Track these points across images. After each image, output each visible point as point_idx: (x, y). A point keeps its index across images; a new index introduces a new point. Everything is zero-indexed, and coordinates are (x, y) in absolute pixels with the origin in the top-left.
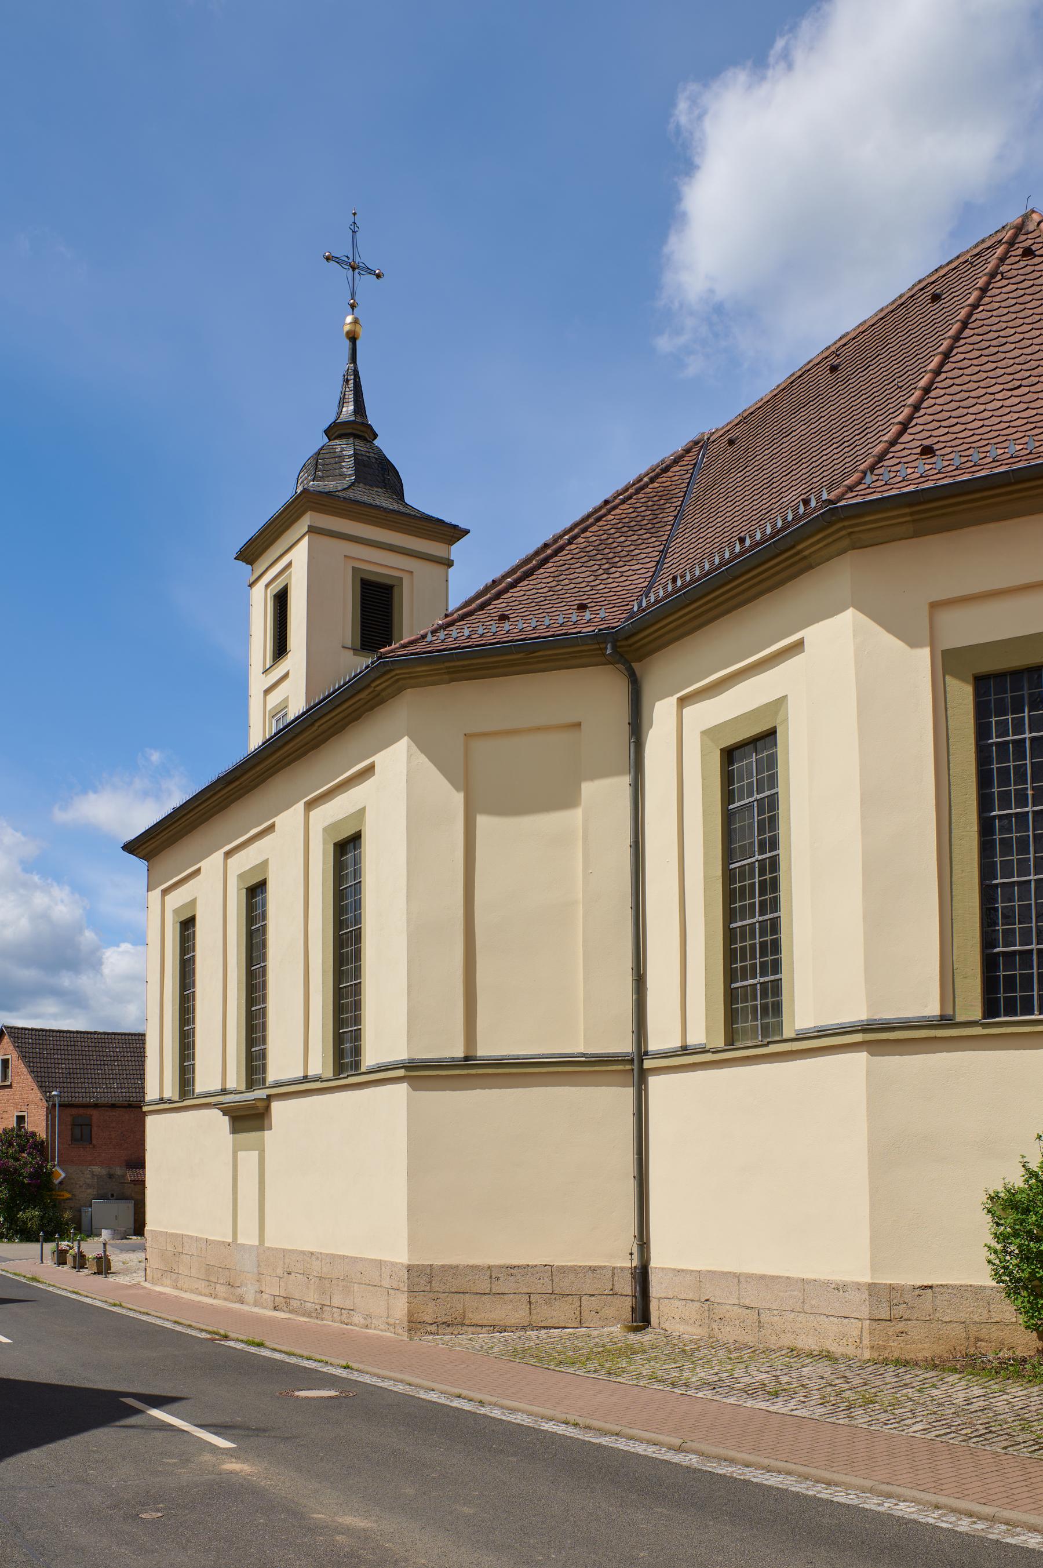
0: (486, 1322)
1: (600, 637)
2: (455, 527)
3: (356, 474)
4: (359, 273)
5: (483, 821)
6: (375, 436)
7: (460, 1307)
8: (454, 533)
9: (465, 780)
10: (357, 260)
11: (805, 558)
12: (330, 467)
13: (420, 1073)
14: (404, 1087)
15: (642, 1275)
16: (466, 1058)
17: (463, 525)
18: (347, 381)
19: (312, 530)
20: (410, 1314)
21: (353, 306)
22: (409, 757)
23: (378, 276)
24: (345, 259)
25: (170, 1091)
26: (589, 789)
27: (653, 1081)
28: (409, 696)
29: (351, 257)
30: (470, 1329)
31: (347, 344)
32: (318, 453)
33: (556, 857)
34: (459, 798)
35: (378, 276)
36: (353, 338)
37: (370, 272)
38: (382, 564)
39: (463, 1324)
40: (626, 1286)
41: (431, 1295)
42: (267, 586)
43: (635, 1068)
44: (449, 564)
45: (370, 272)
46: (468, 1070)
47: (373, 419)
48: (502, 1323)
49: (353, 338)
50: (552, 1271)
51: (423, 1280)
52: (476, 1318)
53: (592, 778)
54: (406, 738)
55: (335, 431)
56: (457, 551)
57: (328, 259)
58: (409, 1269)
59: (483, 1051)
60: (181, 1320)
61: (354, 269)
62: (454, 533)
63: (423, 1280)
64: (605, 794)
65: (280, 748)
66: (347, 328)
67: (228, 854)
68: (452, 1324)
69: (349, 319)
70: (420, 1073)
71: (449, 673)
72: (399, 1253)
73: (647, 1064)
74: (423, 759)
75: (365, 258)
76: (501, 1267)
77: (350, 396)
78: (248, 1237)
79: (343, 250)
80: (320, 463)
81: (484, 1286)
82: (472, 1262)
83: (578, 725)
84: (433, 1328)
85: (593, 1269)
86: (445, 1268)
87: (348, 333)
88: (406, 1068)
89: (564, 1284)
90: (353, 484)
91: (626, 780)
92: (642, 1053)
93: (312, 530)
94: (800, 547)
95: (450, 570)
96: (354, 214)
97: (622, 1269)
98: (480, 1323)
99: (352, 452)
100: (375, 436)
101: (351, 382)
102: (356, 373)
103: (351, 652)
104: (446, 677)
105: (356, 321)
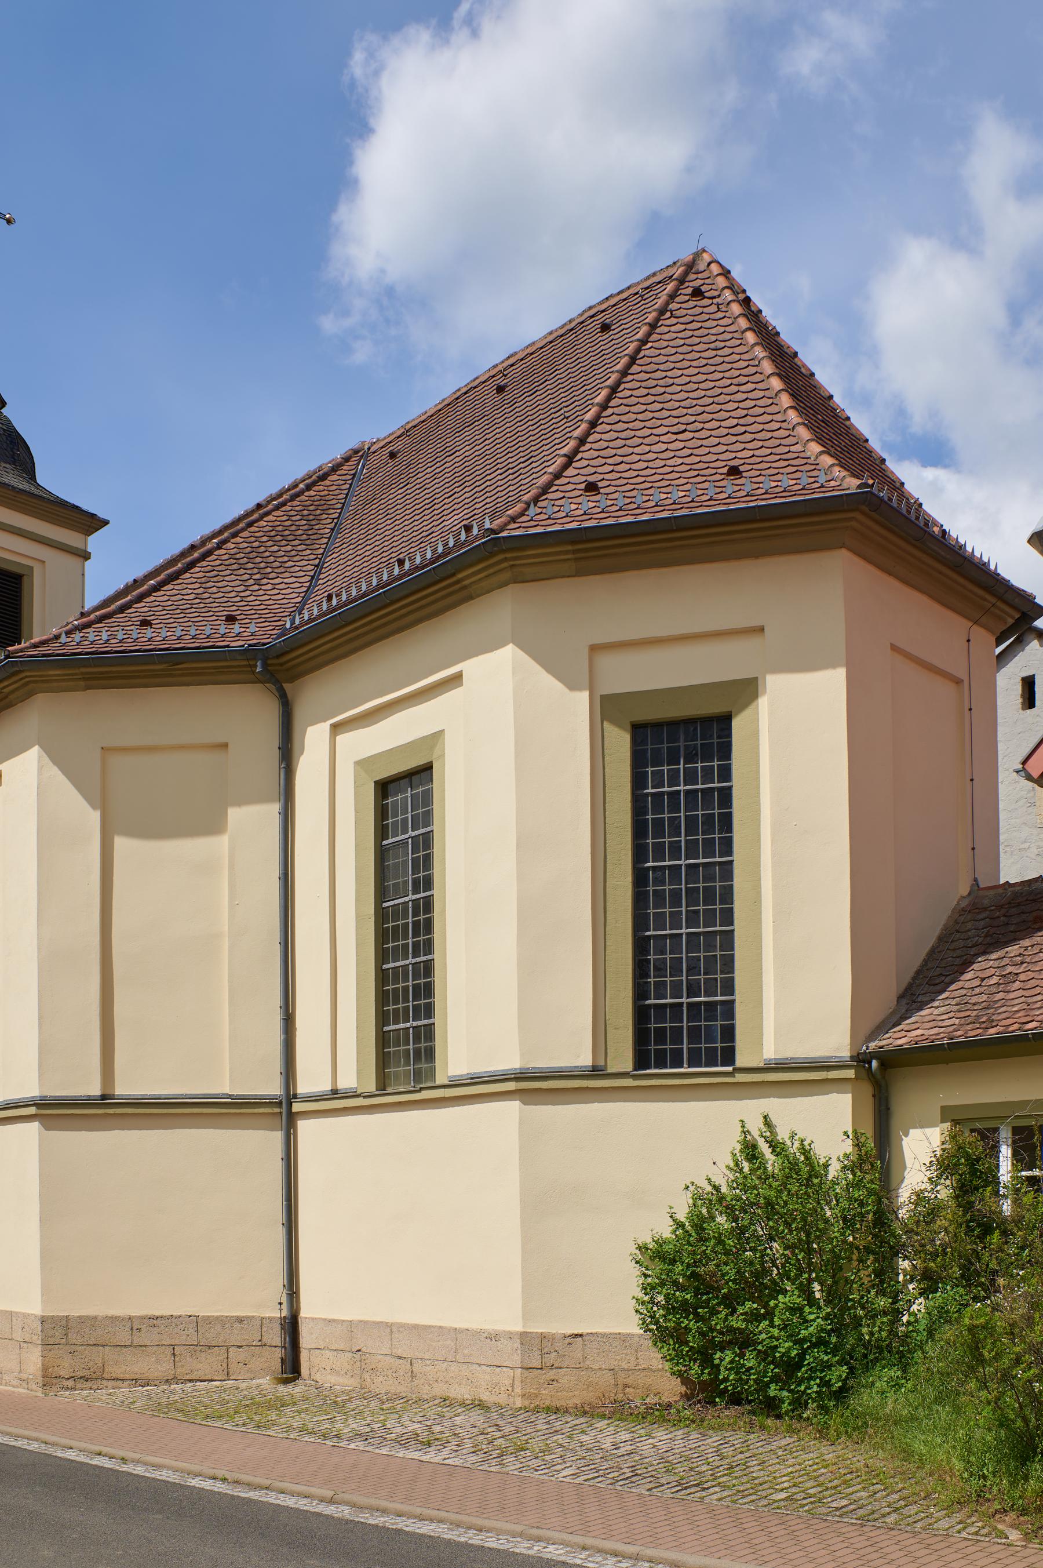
0: (127, 1376)
1: (250, 653)
5: (121, 844)
9: (102, 799)
14: (35, 1126)
15: (292, 1325)
16: (104, 1097)
17: (102, 514)
26: (235, 815)
27: (302, 1125)
30: (111, 1383)
34: (95, 816)
39: (102, 1379)
40: (275, 1336)
41: (69, 1348)
43: (283, 1111)
44: (86, 556)
52: (118, 1371)
53: (239, 803)
56: (94, 542)
58: (43, 1320)
59: (121, 1089)
62: (92, 523)
63: (59, 1333)
71: (84, 679)
74: (55, 772)
76: (142, 1318)
81: (124, 1338)
82: (111, 1312)
83: (225, 746)
84: (70, 1383)
85: (240, 1320)
86: (82, 1320)
89: (210, 1336)
91: (276, 808)
92: (291, 1096)
94: (460, 576)
97: (271, 1319)
98: (121, 1376)
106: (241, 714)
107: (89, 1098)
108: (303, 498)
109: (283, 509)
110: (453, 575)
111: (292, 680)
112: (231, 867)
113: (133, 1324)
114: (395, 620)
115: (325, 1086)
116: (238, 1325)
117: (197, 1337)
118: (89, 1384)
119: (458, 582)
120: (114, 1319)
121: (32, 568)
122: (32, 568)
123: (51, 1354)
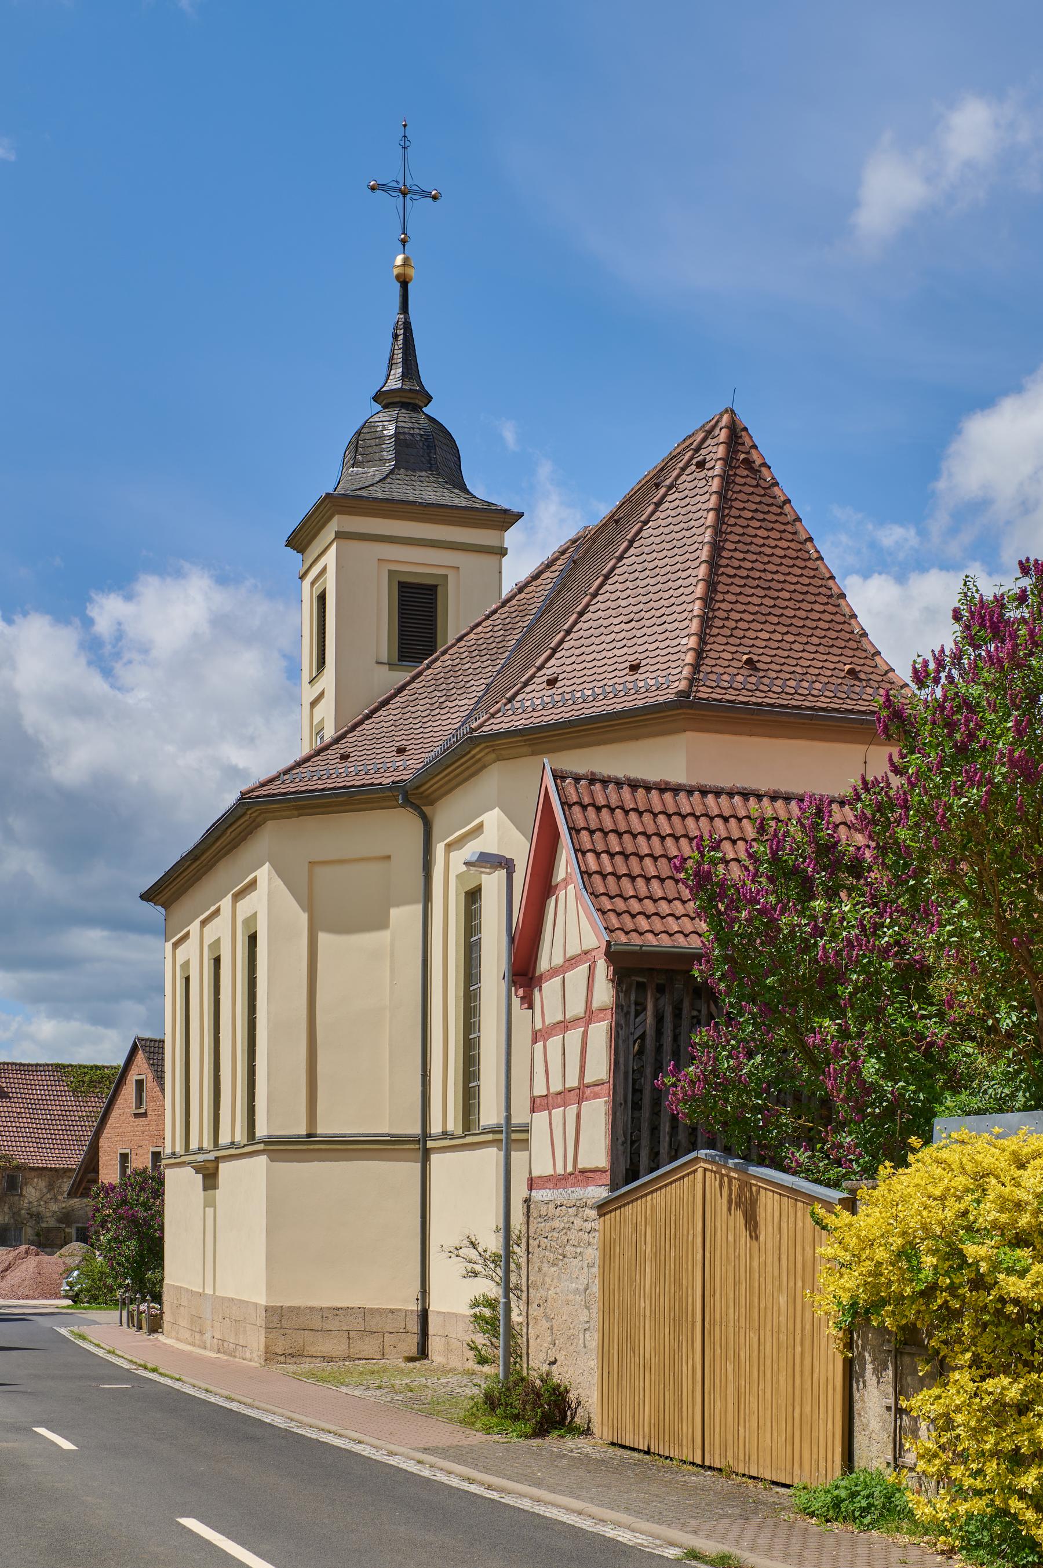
0: (319, 1354)
1: (394, 786)
2: (506, 511)
3: (396, 458)
4: (412, 199)
5: (323, 937)
6: (429, 399)
7: (301, 1341)
8: (506, 518)
9: (309, 904)
10: (408, 184)
11: (480, 759)
12: (370, 449)
13: (280, 1148)
14: (263, 1159)
15: (424, 1316)
16: (309, 1136)
17: (515, 509)
18: (396, 337)
19: (340, 535)
20: (267, 1347)
21: (404, 242)
22: (270, 879)
23: (435, 198)
24: (395, 184)
25: (453, 1125)
26: (394, 913)
27: (434, 1157)
28: (270, 824)
29: (402, 183)
30: (308, 1360)
31: (397, 287)
32: (359, 433)
33: (376, 969)
34: (304, 917)
35: (435, 198)
36: (404, 283)
37: (425, 194)
38: (421, 563)
39: (303, 1356)
40: (414, 1326)
41: (282, 1331)
42: (313, 584)
43: (421, 1147)
44: (502, 552)
45: (425, 194)
46: (309, 1145)
47: (429, 379)
48: (329, 1355)
49: (404, 283)
50: (364, 1312)
51: (277, 1318)
52: (312, 1350)
53: (398, 905)
54: (267, 864)
55: (384, 399)
56: (512, 537)
57: (373, 189)
58: (267, 1309)
59: (323, 1129)
60: (233, 1396)
61: (404, 194)
62: (506, 518)
63: (276, 1319)
64: (405, 916)
65: (218, 839)
66: (396, 271)
67: (204, 923)
68: (295, 1355)
69: (399, 260)
70: (280, 1148)
71: (297, 809)
72: (262, 1301)
73: (430, 1144)
74: (279, 882)
75: (419, 179)
76: (329, 1308)
77: (399, 356)
78: (209, 1291)
79: (391, 175)
80: (361, 446)
81: (317, 1324)
82: (310, 1304)
83: (389, 857)
84: (282, 1359)
85: (392, 1312)
86: (291, 1309)
87: (398, 277)
88: (265, 1143)
89: (373, 1323)
90: (392, 472)
91: (419, 908)
92: (425, 1135)
93: (340, 535)
94: (473, 752)
95: (504, 559)
96: (405, 126)
97: (412, 1311)
98: (315, 1354)
99: (392, 432)
100: (429, 399)
101: (401, 337)
102: (407, 326)
103: (387, 667)
104: (296, 813)
105: (406, 262)
106: (398, 829)
107: (299, 1136)
108: (514, 602)
109: (553, 569)
110: (469, 752)
111: (432, 803)
112: (392, 955)
113: (324, 1313)
114: (446, 783)
115: (560, 1088)
116: (390, 1315)
117: (364, 1322)
118: (294, 1360)
119: (473, 756)
120: (311, 1309)
121: (446, 576)
122: (446, 576)
123: (271, 1336)
